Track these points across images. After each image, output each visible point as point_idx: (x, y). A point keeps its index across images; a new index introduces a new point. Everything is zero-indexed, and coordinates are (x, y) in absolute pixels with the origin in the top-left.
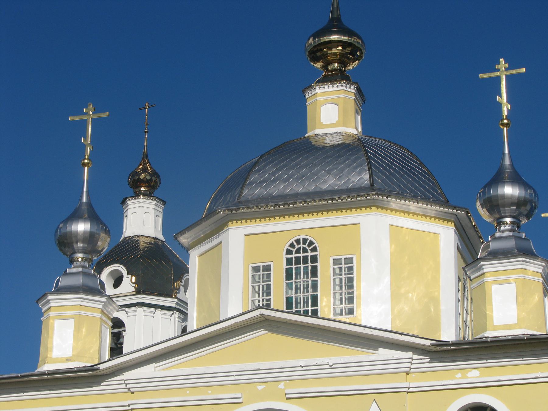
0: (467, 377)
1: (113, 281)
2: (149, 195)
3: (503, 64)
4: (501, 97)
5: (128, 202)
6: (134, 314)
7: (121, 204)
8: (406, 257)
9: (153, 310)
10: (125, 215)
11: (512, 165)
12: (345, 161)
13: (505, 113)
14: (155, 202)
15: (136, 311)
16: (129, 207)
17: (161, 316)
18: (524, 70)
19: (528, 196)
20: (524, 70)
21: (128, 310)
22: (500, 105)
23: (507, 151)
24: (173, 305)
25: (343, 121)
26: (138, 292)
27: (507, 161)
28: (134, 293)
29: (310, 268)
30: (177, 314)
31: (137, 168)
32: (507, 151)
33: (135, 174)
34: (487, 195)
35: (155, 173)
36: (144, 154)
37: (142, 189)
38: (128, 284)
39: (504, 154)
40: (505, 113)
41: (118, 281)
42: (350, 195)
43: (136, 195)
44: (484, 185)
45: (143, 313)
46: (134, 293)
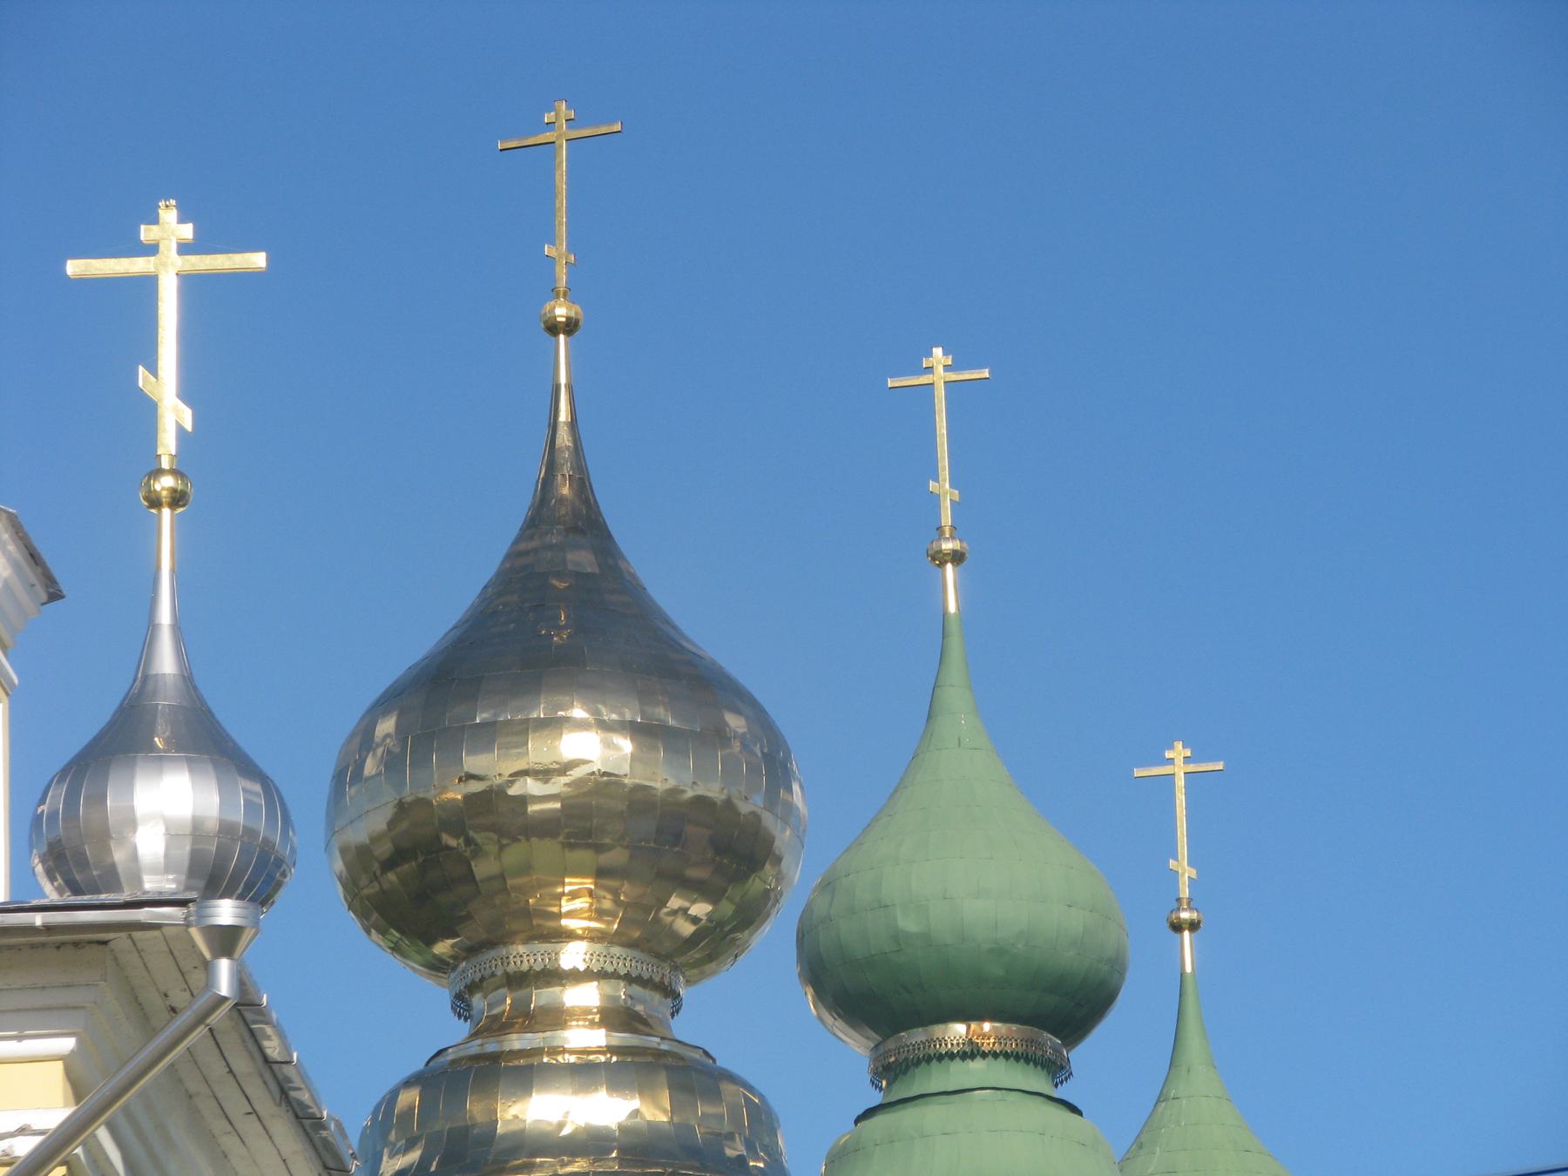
0: (61, 1164)
3: (170, 226)
4: (155, 374)
8: (671, 722)
11: (187, 678)
12: (538, 1052)
13: (167, 445)
18: (258, 260)
19: (239, 817)
20: (258, 260)
22: (149, 409)
23: (165, 615)
25: (507, 1122)
27: (166, 662)
29: (1180, 782)
32: (165, 615)
34: (442, 1125)
39: (152, 627)
40: (167, 445)
44: (345, 1125)
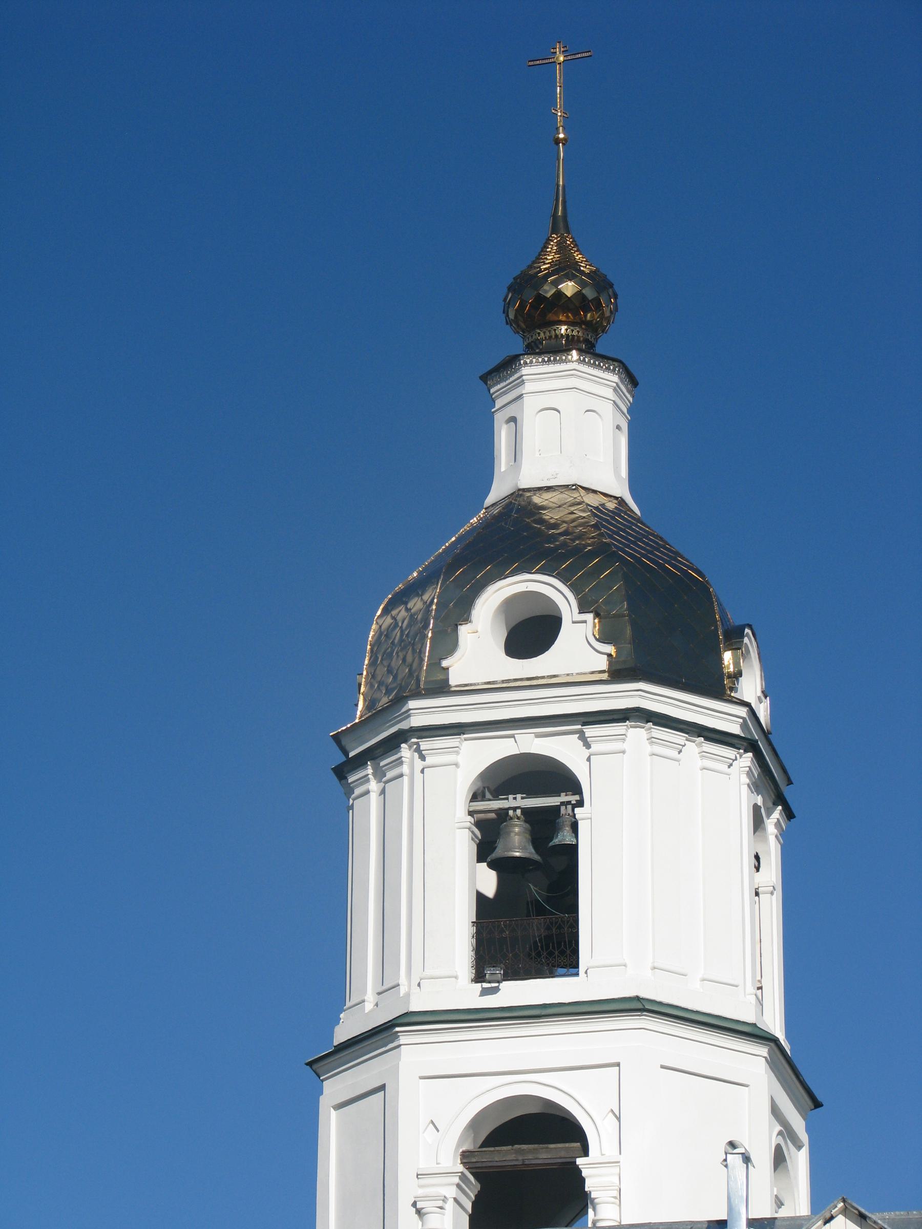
1: (506, 635)
2: (589, 351)
5: (525, 371)
6: (617, 746)
7: (481, 378)
9: (678, 737)
10: (500, 419)
14: (616, 378)
15: (623, 737)
16: (528, 387)
17: (700, 763)
21: (591, 731)
24: (735, 729)
26: (619, 673)
28: (605, 676)
30: (747, 759)
31: (539, 258)
33: (526, 282)
35: (600, 281)
36: (555, 215)
37: (563, 329)
38: (579, 646)
41: (531, 633)
42: (553, 341)
43: (555, 350)
45: (649, 749)
46: (605, 676)
